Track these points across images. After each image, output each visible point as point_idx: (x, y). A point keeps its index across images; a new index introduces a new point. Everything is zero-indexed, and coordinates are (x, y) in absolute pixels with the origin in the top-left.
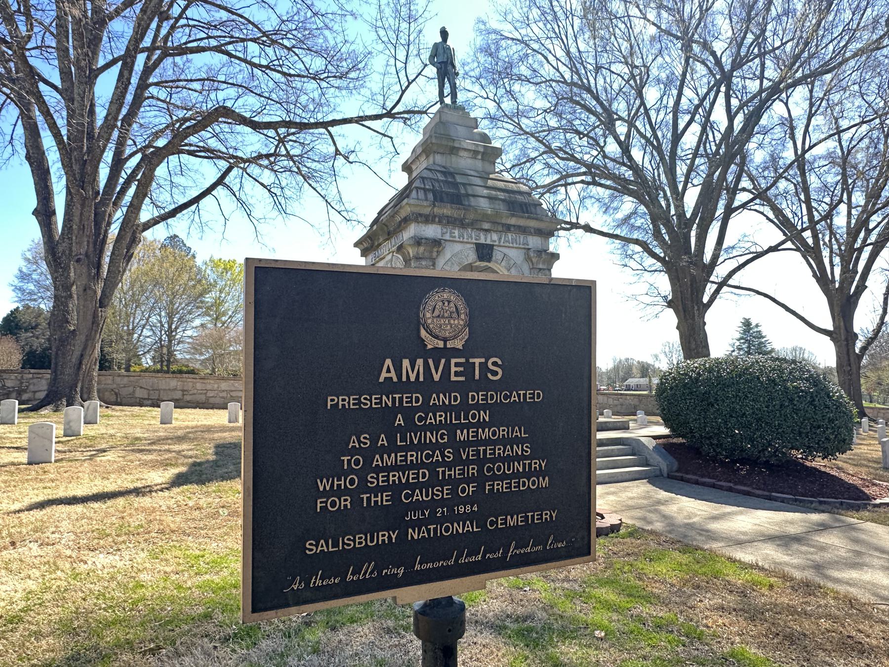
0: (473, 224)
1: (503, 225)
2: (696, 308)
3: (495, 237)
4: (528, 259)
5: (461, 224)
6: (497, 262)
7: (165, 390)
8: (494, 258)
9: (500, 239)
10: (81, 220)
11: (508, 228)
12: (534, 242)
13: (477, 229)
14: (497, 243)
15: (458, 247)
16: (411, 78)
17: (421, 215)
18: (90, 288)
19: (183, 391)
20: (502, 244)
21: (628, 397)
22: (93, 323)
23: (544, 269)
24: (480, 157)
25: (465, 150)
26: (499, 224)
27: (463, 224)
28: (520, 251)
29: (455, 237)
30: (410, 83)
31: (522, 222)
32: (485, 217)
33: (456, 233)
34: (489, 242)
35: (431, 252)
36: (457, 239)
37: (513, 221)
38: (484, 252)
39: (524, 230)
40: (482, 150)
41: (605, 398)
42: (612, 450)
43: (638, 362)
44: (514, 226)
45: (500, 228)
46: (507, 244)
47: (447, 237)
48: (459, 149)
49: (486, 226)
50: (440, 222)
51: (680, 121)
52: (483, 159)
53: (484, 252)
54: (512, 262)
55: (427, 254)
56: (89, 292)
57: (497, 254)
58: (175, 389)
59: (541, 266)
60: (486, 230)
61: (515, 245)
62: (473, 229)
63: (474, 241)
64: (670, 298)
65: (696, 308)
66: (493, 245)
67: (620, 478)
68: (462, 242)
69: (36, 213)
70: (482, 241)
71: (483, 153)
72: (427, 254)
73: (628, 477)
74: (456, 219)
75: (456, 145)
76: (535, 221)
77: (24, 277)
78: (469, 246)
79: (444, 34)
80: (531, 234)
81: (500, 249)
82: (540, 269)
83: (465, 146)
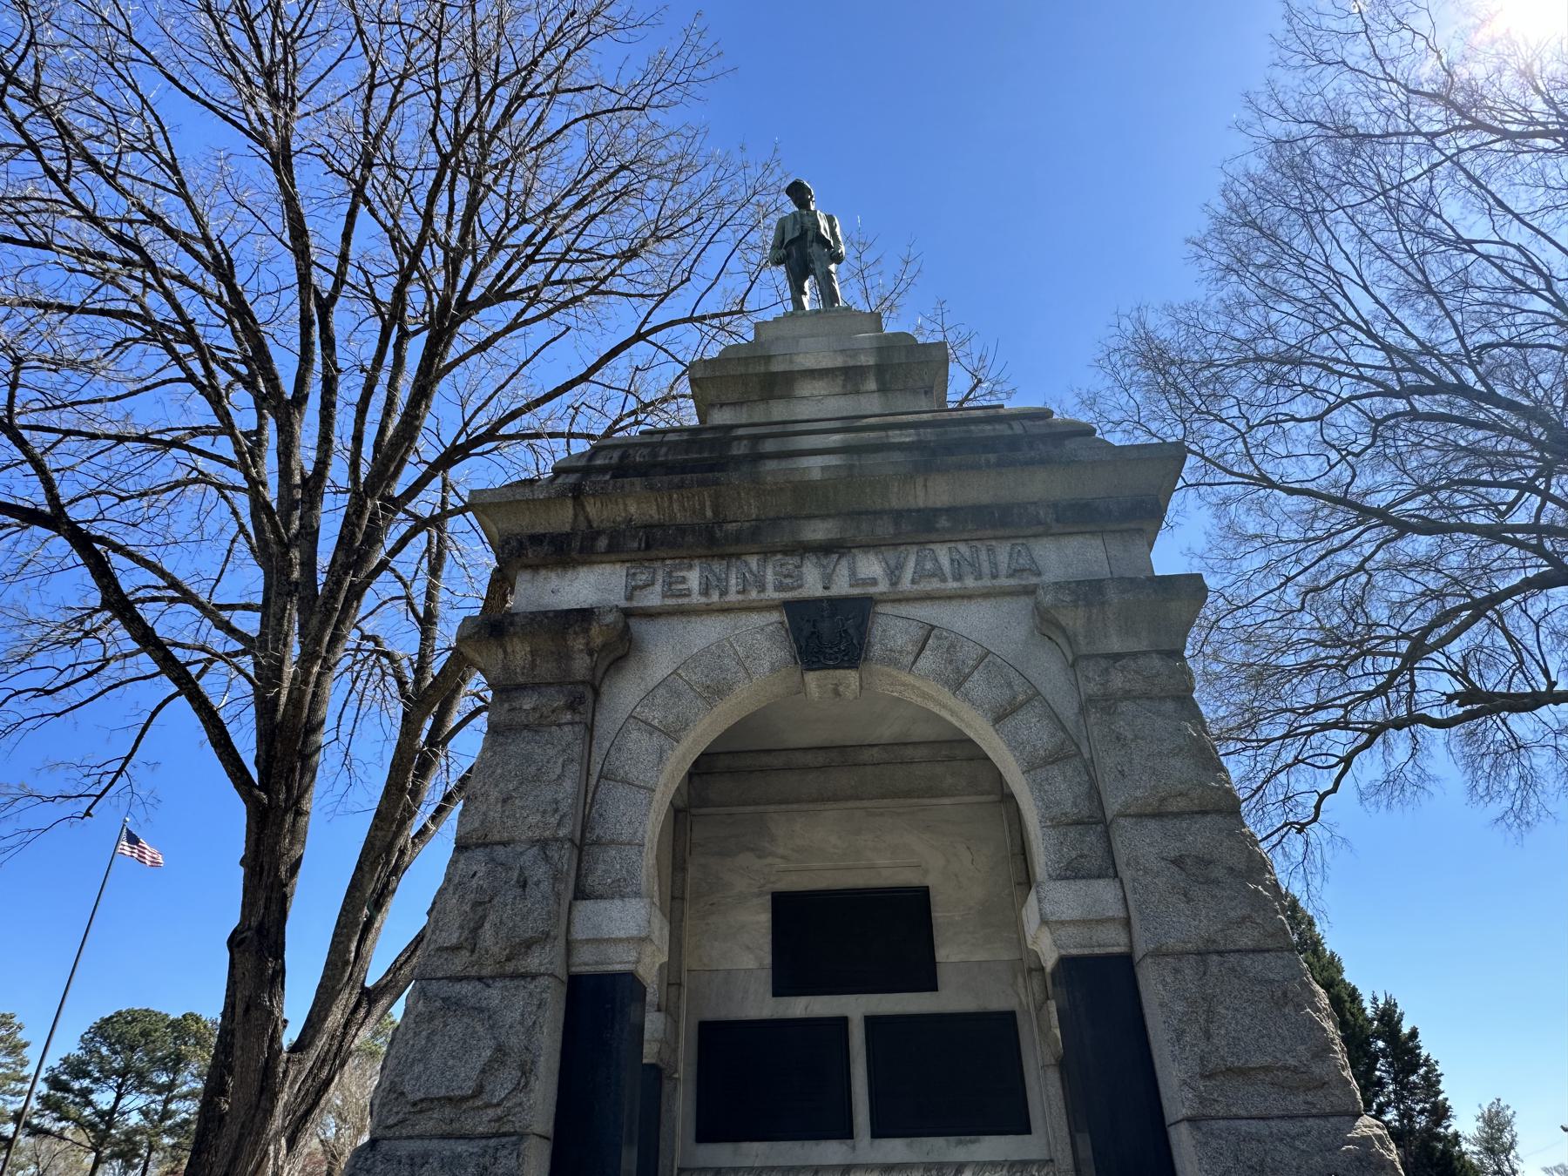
0: (766, 537)
1: (898, 515)
3: (871, 566)
4: (1046, 625)
5: (714, 542)
6: (894, 662)
8: (877, 650)
9: (894, 574)
11: (921, 527)
12: (1061, 559)
13: (788, 551)
14: (883, 587)
15: (705, 633)
17: (536, 539)
20: (906, 584)
22: (262, 1090)
24: (872, 385)
25: (813, 374)
26: (878, 514)
27: (712, 541)
28: (1007, 605)
29: (688, 594)
33: (694, 578)
34: (842, 586)
35: (564, 656)
36: (696, 599)
38: (828, 635)
43: (1332, 953)
44: (951, 511)
45: (885, 529)
46: (934, 585)
47: (653, 598)
49: (817, 531)
52: (883, 389)
53: (828, 635)
54: (969, 653)
55: (547, 669)
56: (254, 1014)
57: (892, 631)
59: (1116, 645)
61: (970, 582)
62: (766, 554)
63: (771, 594)
68: (726, 610)
71: (881, 370)
72: (547, 669)
74: (682, 530)
75: (777, 367)
78: (757, 619)
79: (798, 192)
81: (904, 610)
82: (1116, 657)
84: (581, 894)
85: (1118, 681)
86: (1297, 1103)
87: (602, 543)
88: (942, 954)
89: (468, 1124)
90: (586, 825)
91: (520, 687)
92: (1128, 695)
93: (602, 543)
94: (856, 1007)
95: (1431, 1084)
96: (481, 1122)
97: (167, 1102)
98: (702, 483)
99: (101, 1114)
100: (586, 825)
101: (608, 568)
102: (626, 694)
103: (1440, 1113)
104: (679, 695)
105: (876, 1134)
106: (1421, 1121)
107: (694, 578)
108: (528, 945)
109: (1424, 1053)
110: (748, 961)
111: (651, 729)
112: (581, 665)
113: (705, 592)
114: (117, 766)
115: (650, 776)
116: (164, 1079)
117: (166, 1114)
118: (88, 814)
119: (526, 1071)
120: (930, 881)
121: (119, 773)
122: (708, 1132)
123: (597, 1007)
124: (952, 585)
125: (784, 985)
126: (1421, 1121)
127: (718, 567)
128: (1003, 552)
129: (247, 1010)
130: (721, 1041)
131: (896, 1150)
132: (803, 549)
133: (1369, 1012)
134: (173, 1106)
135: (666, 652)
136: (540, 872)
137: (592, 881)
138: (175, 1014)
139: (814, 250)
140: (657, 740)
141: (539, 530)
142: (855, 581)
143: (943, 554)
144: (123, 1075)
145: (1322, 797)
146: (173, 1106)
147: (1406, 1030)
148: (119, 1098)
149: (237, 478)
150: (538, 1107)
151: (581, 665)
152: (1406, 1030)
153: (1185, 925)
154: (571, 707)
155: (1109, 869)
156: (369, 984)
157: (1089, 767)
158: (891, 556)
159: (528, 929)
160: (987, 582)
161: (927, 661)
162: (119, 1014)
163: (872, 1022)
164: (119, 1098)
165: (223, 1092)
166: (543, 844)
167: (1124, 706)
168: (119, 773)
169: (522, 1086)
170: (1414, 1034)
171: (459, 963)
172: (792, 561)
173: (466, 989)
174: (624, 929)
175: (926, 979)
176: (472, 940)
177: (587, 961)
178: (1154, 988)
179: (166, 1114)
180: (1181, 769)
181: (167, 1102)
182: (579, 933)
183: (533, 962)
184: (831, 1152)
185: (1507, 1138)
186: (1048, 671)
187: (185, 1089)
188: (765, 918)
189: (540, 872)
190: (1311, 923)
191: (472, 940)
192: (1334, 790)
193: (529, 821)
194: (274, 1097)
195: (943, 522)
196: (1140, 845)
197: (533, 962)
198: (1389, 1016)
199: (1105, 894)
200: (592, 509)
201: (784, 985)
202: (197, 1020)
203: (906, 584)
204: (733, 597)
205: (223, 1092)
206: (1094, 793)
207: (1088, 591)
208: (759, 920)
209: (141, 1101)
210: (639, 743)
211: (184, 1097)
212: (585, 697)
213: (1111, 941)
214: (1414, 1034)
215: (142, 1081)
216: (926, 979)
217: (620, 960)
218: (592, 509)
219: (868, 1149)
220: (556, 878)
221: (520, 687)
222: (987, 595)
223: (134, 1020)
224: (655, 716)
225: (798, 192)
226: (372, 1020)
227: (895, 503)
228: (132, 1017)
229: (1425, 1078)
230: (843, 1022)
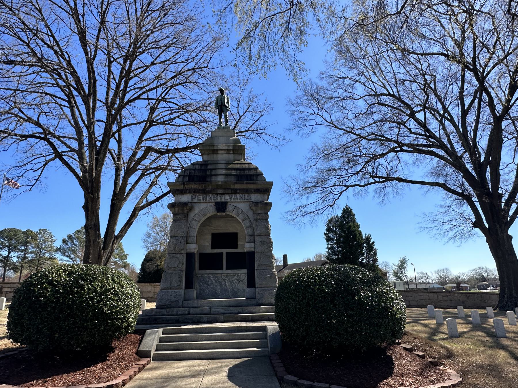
0: (213, 191)
1: (232, 189)
2: (498, 226)
3: (227, 197)
5: (204, 192)
7: (145, 292)
9: (231, 198)
10: (92, 208)
11: (235, 191)
12: (255, 197)
14: (229, 201)
15: (203, 206)
16: (241, 115)
17: (178, 190)
18: (96, 241)
19: (154, 292)
20: (232, 200)
21: (456, 295)
22: (99, 258)
23: (261, 213)
24: (232, 152)
27: (204, 192)
28: (246, 203)
30: (240, 117)
31: (244, 186)
32: (219, 187)
33: (201, 197)
34: (223, 200)
35: (183, 210)
36: (202, 201)
37: (238, 186)
38: (221, 207)
39: (247, 191)
40: (231, 148)
41: (436, 295)
42: (248, 335)
44: (239, 189)
45: (230, 192)
46: (236, 201)
47: (195, 200)
48: (217, 150)
49: (220, 191)
50: (190, 193)
51: (465, 102)
52: (234, 153)
55: (181, 212)
56: (95, 243)
57: (230, 208)
58: (150, 292)
59: (259, 212)
60: (221, 194)
61: (241, 200)
62: (212, 194)
63: (213, 201)
64: (474, 220)
65: (498, 226)
66: (227, 202)
67: (231, 355)
69: (83, 207)
70: (219, 200)
71: (233, 150)
72: (181, 212)
73: (238, 355)
75: (215, 148)
76: (253, 185)
77: (148, 235)
78: (211, 204)
80: (252, 193)
81: (232, 204)
82: (259, 213)
83: (221, 148)
84: (187, 243)
85: (258, 217)
86: (268, 268)
87: (188, 191)
88: (238, 243)
89: (176, 269)
90: (187, 233)
91: (177, 214)
92: (260, 219)
93: (188, 191)
94: (224, 251)
95: (375, 255)
96: (178, 269)
97: (25, 254)
98: (203, 184)
99: (4, 258)
100: (187, 233)
101: (188, 195)
102: (192, 215)
103: (376, 260)
104: (199, 215)
105: (226, 269)
106: (371, 262)
107: (201, 197)
108: (182, 250)
109: (375, 247)
110: (207, 244)
111: (196, 220)
112: (186, 211)
113: (203, 200)
114: (37, 178)
115: (196, 226)
116: (23, 248)
117: (25, 258)
118: (30, 190)
119: (183, 264)
120: (238, 232)
121: (37, 180)
122: (201, 268)
123: (190, 256)
124: (239, 201)
125: (213, 247)
126: (371, 262)
127: (205, 196)
128: (246, 195)
129: (94, 242)
130: (203, 256)
131: (229, 271)
132: (217, 194)
133: (364, 237)
134: (27, 256)
135: (197, 209)
136: (182, 241)
137: (189, 241)
138: (24, 230)
139: (224, 108)
140: (197, 222)
141: (178, 188)
142: (225, 199)
143: (238, 195)
144: (9, 247)
145: (336, 200)
146: (27, 256)
147: (372, 242)
148: (9, 253)
149: (67, 104)
150: (184, 268)
151: (186, 211)
152: (372, 242)
153: (260, 249)
154: (185, 217)
155: (254, 242)
156: (116, 235)
157: (254, 228)
158: (230, 195)
159: (182, 248)
160: (243, 201)
161: (234, 212)
162: (5, 229)
163: (227, 253)
164: (9, 253)
165: (89, 258)
166: (182, 237)
167: (259, 221)
168: (37, 180)
169: (182, 266)
170: (373, 243)
171: (173, 252)
172: (216, 196)
173: (174, 255)
174: (193, 248)
175: (236, 247)
176: (175, 249)
177: (188, 251)
178: (256, 256)
179: (25, 258)
180: (264, 230)
181: (25, 254)
182: (187, 248)
183: (182, 252)
184: (220, 271)
185: (405, 265)
186: (250, 214)
187: (30, 251)
188: (210, 237)
189: (182, 241)
190: (354, 215)
191: (175, 249)
192: (338, 199)
193: (180, 234)
194: (101, 259)
195: (238, 191)
196: (257, 239)
197: (182, 252)
198: (368, 239)
199: (252, 245)
200: (186, 186)
201: (213, 247)
202: (31, 231)
203: (232, 200)
204: (207, 201)
205: (89, 258)
206: (254, 232)
207: (256, 203)
208: (210, 237)
209: (16, 254)
210: (194, 222)
211: (31, 253)
212: (186, 216)
213: (253, 250)
214: (373, 243)
215: (16, 249)
216: (236, 247)
217: (193, 251)
218: (186, 186)
219: (225, 271)
220: (184, 241)
221: (177, 214)
222: (244, 202)
223: (11, 231)
224: (196, 218)
225: (222, 91)
226: (117, 243)
227: (231, 188)
228: (10, 230)
229: (374, 253)
230: (222, 253)
